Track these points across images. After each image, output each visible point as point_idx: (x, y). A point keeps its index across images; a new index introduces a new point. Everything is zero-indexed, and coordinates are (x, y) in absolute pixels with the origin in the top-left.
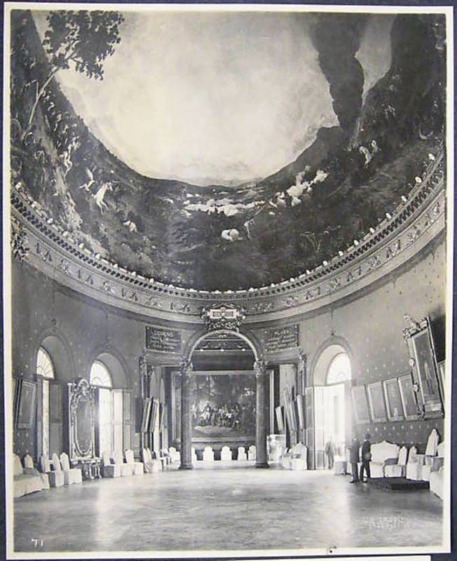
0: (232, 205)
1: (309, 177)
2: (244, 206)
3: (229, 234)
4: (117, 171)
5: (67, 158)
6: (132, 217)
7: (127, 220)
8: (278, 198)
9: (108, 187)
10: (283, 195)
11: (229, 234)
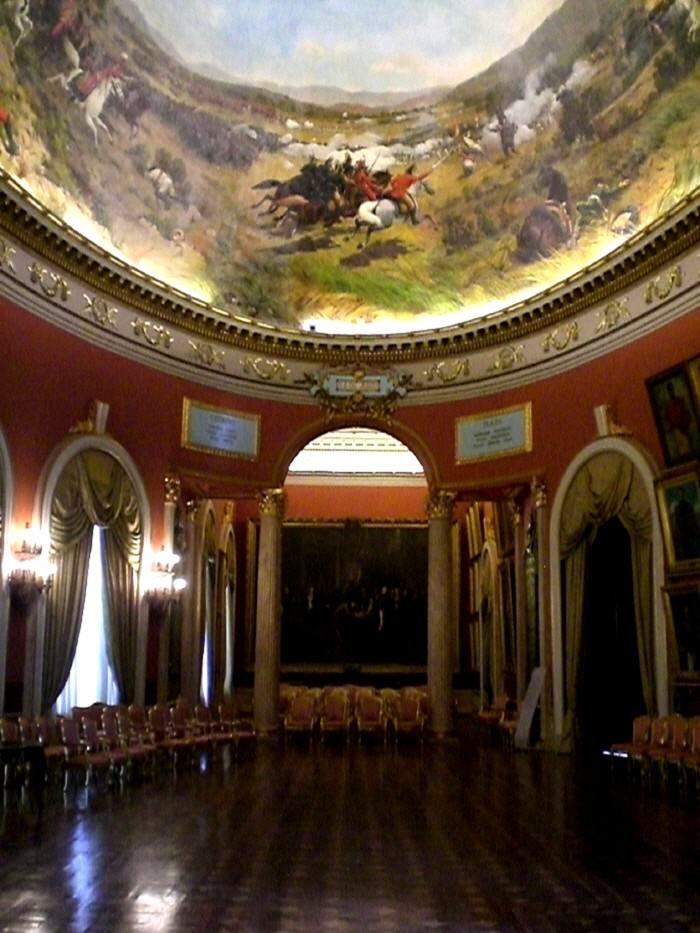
0: (383, 148)
1: (552, 79)
2: (407, 150)
3: (374, 212)
4: (134, 55)
5: (23, 9)
6: (163, 163)
7: (153, 168)
8: (485, 130)
9: (115, 88)
10: (495, 123)
11: (374, 212)
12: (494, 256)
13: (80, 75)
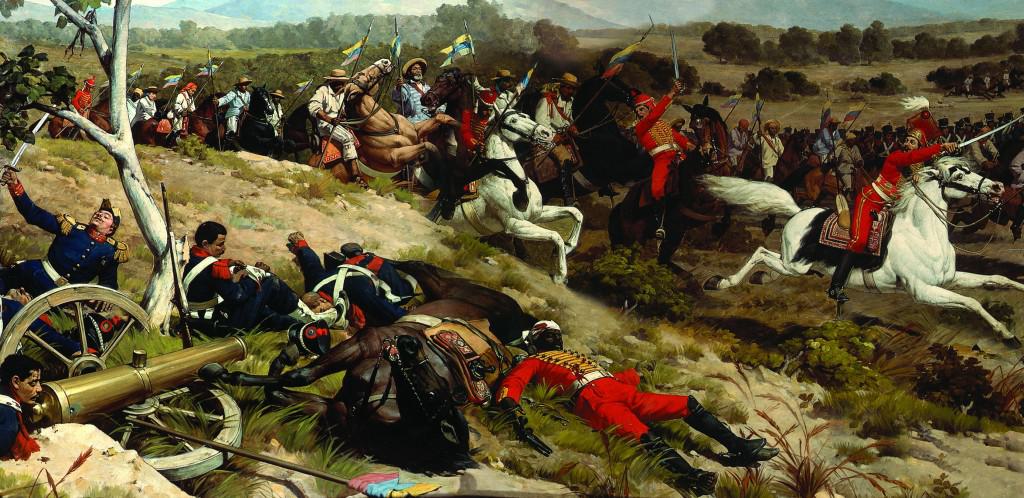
12: (230, 60)
13: (818, 222)
